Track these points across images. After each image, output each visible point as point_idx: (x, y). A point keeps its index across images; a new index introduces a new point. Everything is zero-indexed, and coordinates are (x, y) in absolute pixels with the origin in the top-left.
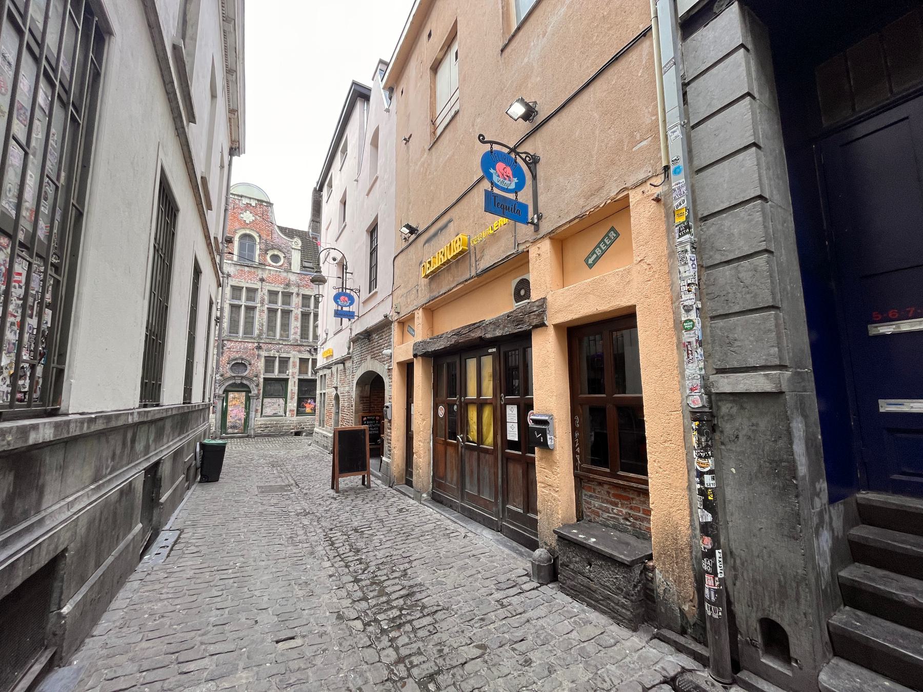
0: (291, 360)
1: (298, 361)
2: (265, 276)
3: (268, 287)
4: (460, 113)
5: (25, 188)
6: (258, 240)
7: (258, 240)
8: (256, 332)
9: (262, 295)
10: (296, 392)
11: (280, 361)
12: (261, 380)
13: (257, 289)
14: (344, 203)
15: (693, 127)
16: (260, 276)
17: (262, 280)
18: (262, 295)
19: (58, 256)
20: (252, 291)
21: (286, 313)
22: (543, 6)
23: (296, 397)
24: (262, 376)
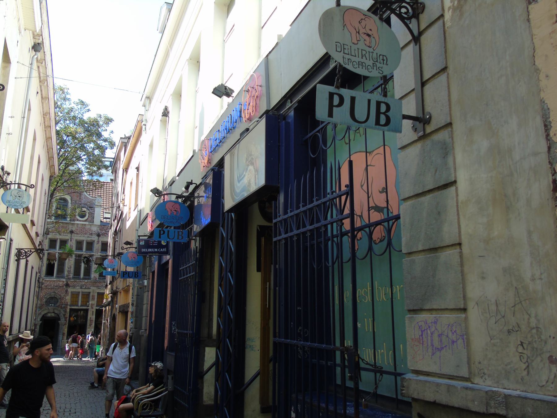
0: (91, 294)
1: (96, 294)
2: (74, 229)
3: (76, 237)
4: (279, 45)
5: (3, 292)
6: (70, 201)
7: (70, 201)
8: (66, 273)
9: (71, 245)
10: (94, 320)
11: (82, 295)
12: (68, 310)
13: (68, 240)
14: (151, 146)
15: (384, 132)
16: (70, 229)
17: (72, 232)
18: (71, 245)
19: (3, 301)
20: (64, 243)
21: (88, 261)
22: (311, 2)
23: (93, 325)
24: (69, 307)
